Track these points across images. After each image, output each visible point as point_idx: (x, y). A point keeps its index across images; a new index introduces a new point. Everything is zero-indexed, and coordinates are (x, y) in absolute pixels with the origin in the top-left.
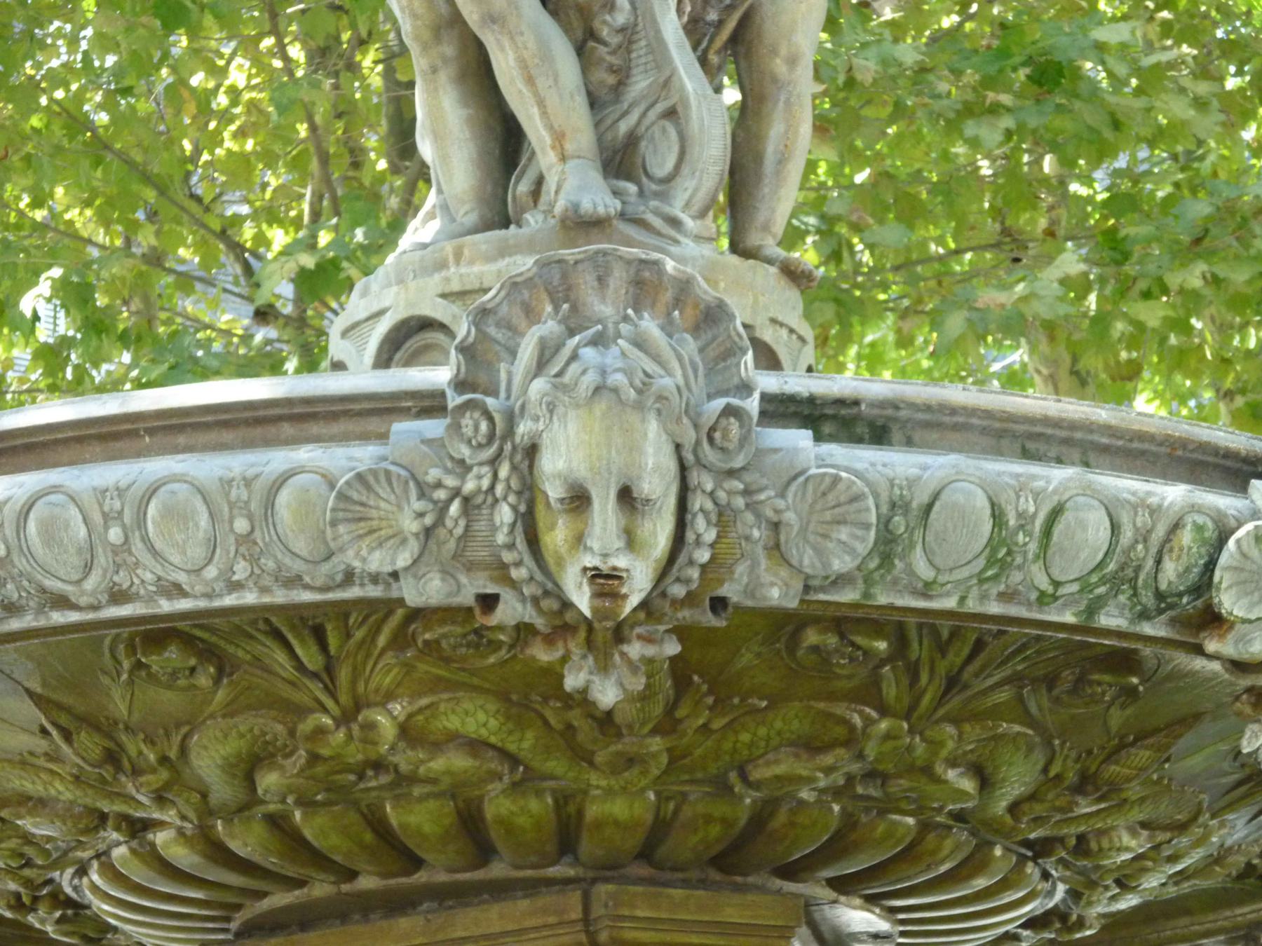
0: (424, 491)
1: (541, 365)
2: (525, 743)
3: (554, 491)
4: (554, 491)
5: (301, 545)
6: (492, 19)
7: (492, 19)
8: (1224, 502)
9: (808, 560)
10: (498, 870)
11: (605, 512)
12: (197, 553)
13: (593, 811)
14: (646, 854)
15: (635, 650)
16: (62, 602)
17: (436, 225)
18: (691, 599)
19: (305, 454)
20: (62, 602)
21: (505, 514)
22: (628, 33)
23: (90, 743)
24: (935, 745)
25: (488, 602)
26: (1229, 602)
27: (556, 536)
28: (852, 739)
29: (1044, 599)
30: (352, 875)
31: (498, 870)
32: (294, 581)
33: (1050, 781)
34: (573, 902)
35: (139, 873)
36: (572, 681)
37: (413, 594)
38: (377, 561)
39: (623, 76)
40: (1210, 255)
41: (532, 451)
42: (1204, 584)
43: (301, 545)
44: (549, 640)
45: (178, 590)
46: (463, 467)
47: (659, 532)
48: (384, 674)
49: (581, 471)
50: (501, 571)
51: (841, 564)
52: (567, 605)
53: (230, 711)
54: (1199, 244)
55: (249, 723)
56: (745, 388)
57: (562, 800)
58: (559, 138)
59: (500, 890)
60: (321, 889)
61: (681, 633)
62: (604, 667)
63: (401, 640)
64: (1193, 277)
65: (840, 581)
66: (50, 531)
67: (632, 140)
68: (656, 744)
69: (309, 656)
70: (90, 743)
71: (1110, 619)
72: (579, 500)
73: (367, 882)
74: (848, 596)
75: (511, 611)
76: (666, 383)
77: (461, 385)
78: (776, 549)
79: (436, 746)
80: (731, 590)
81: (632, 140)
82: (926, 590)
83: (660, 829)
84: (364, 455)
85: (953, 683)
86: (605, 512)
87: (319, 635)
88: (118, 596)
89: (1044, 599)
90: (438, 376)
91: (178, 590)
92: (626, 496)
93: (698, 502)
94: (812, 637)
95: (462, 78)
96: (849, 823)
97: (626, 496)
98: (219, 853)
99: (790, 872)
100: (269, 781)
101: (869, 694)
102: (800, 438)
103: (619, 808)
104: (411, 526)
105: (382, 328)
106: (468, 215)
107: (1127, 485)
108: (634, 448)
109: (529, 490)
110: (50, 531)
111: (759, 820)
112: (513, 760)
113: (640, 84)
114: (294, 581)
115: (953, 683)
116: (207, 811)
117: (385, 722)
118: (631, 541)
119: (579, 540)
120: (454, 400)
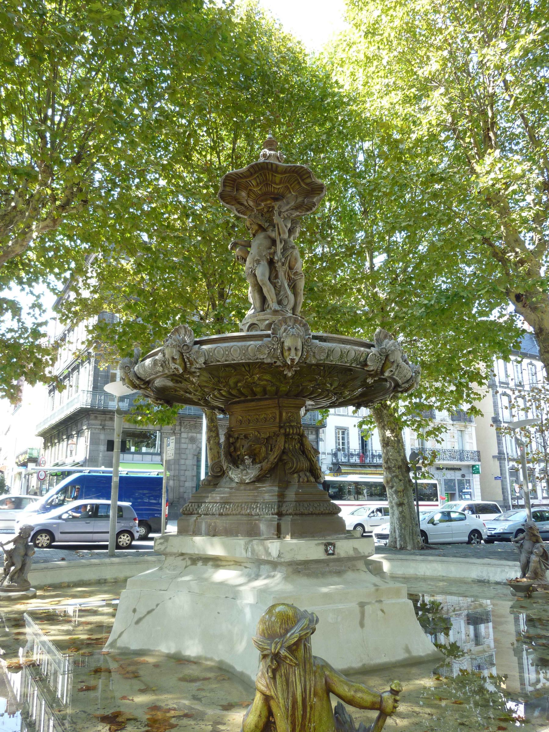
0: (268, 347)
1: (285, 331)
2: (274, 381)
3: (286, 348)
4: (286, 348)
5: (251, 355)
6: (264, 284)
7: (264, 284)
8: (368, 350)
9: (318, 357)
10: (267, 396)
11: (293, 351)
12: (238, 355)
13: (281, 389)
14: (286, 395)
15: (294, 369)
16: (219, 361)
17: (253, 310)
18: (302, 363)
19: (252, 342)
20: (219, 361)
21: (279, 351)
22: (281, 286)
23: (216, 379)
24: (326, 381)
25: (275, 362)
26: (369, 363)
27: (286, 354)
28: (316, 380)
29: (346, 362)
30: (247, 396)
31: (267, 396)
32: (250, 359)
33: (339, 385)
34: (276, 401)
35: (218, 396)
36: (285, 373)
37: (265, 361)
38: (262, 357)
39: (280, 292)
40: (332, 314)
41: (283, 343)
42: (366, 360)
43: (251, 355)
44: (282, 367)
45: (234, 360)
46: (274, 345)
47: (300, 354)
48: (256, 371)
49: (290, 345)
50: (278, 358)
51: (322, 358)
52: (286, 363)
53: (236, 375)
54: (329, 312)
55: (238, 377)
56: (310, 335)
57: (277, 388)
58: (272, 300)
59: (267, 399)
60: (242, 399)
61: (300, 367)
62: (289, 371)
63: (259, 367)
64: (329, 317)
65: (321, 360)
66: (218, 352)
67: (281, 300)
68: (291, 381)
69: (247, 368)
70: (216, 379)
71: (353, 365)
72: (289, 349)
73: (249, 398)
74: (322, 362)
75: (278, 363)
76: (301, 334)
77: (273, 334)
78: (314, 356)
79: (262, 381)
80: (308, 361)
81: (281, 300)
82: (332, 361)
83: (290, 391)
84: (260, 343)
85: (330, 373)
86: (293, 351)
87: (249, 366)
88: (226, 361)
89: (346, 362)
90: (270, 332)
91: (234, 360)
92: (296, 349)
93: (304, 350)
94: (313, 367)
95: (258, 292)
96: (313, 391)
97: (296, 349)
98: (230, 394)
99: (304, 397)
100: (239, 384)
101: (319, 374)
102: (317, 341)
103: (284, 389)
104: (267, 352)
105: (248, 324)
106: (259, 310)
107: (356, 348)
108: (297, 342)
109: (282, 348)
110: (218, 352)
111: (302, 391)
112: (272, 382)
113: (282, 293)
114: (250, 359)
115: (330, 373)
116: (230, 388)
117: (256, 377)
118: (296, 355)
119: (289, 355)
120: (272, 336)
